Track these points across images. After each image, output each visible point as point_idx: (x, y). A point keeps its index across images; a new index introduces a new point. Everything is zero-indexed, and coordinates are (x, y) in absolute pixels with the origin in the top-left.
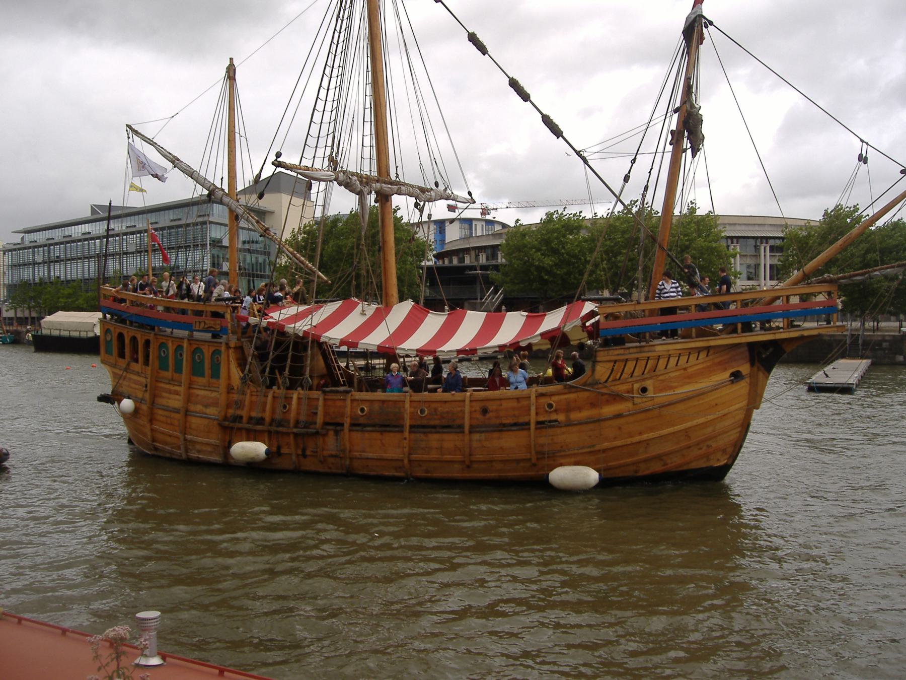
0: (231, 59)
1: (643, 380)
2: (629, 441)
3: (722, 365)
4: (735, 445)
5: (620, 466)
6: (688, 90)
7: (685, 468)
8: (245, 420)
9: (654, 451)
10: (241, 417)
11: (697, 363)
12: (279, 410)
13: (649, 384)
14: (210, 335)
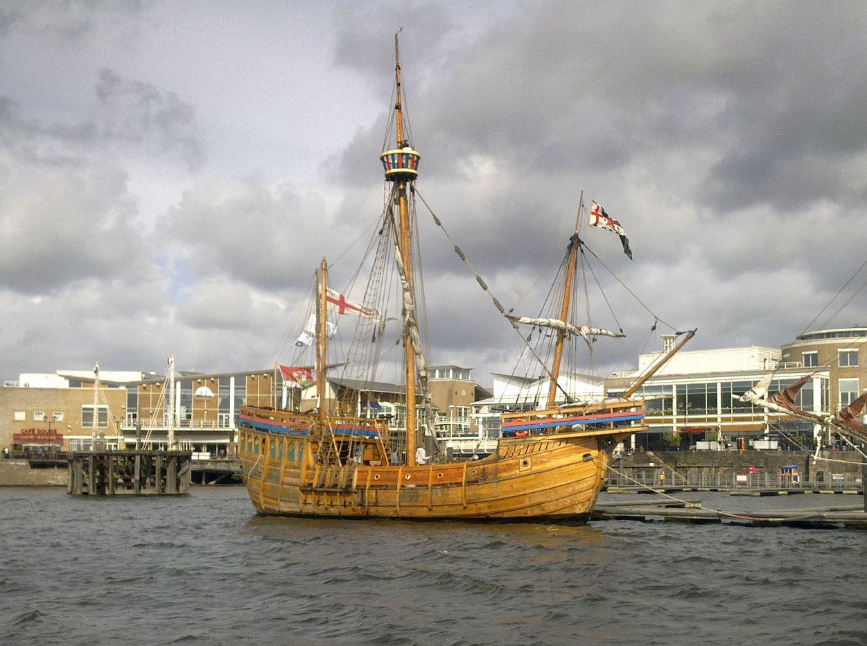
0: (697, 329)
1: (525, 457)
13: (528, 460)
14: (646, 519)
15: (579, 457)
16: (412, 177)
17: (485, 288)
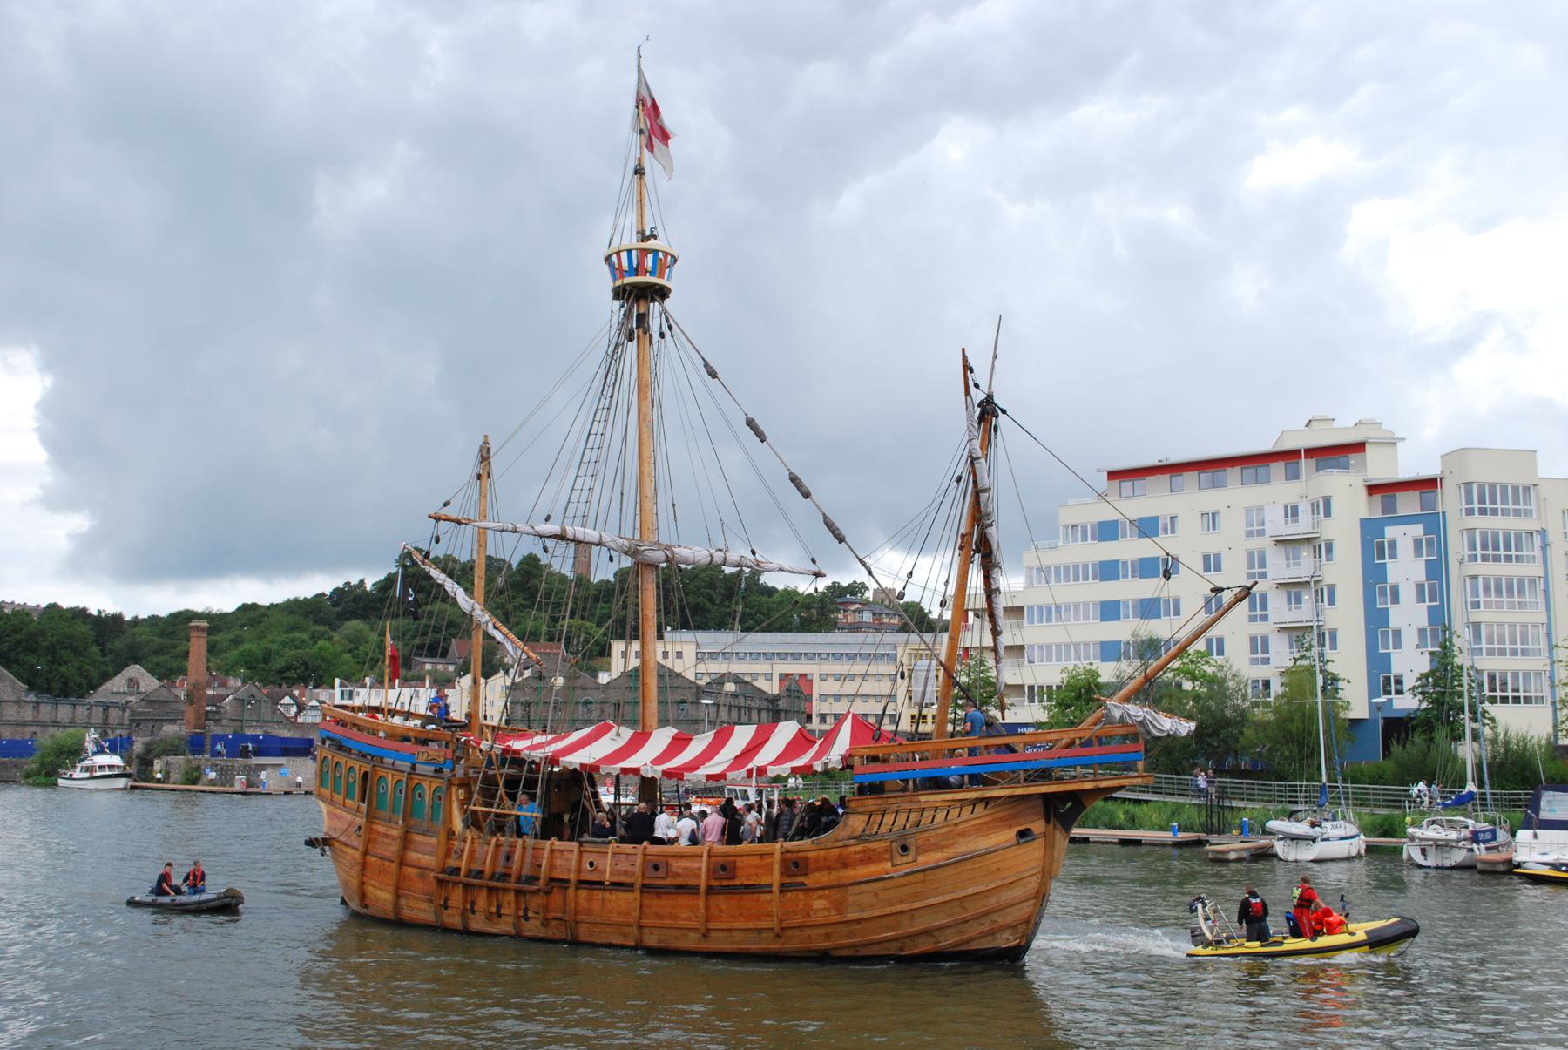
2: (888, 910)
3: (1007, 822)
5: (880, 942)
6: (639, 70)
7: (964, 948)
9: (922, 923)
12: (501, 861)
15: (1010, 834)
16: (662, 293)
17: (807, 495)
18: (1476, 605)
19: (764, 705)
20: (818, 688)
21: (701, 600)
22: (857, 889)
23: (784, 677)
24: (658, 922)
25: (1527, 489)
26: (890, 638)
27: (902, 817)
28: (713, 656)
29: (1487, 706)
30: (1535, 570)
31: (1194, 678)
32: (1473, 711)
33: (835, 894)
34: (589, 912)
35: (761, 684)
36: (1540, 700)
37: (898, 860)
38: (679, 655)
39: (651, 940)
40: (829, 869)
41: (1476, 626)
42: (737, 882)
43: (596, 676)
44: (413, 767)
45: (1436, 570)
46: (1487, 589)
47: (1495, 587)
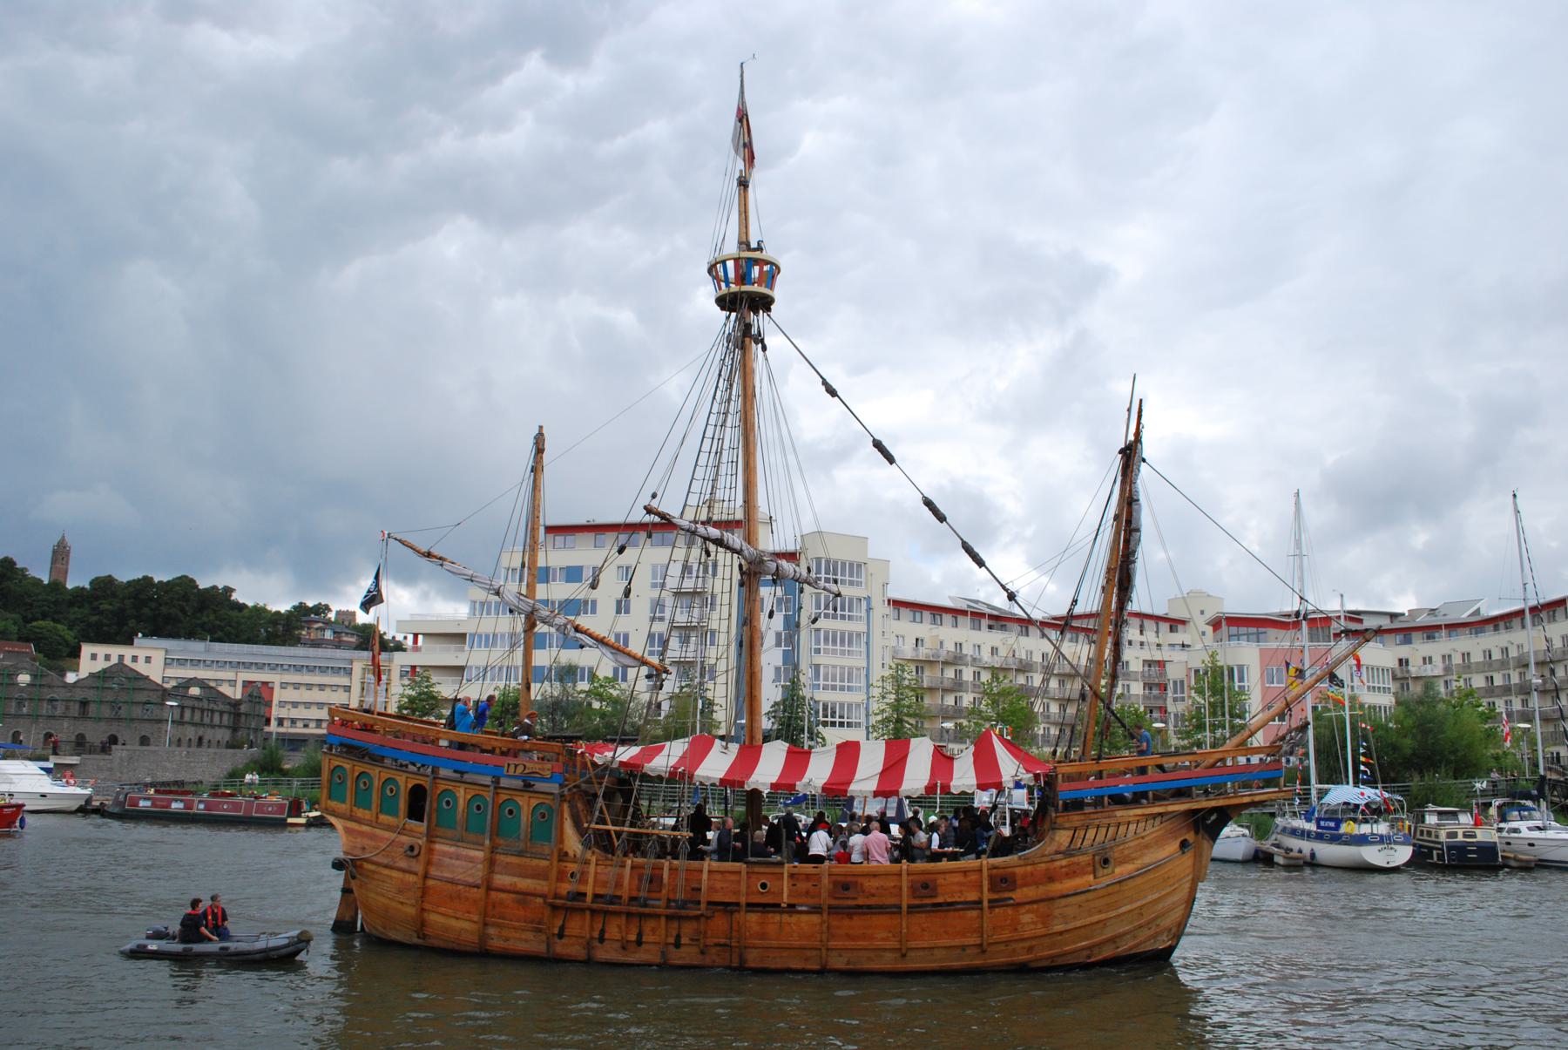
4: (1179, 925)
8: (589, 897)
10: (620, 897)
11: (1152, 830)
18: (818, 651)
19: (227, 708)
20: (279, 694)
21: (173, 611)
22: (1063, 902)
23: (247, 684)
24: (849, 944)
25: (859, 566)
26: (347, 654)
27: (1103, 831)
28: (182, 662)
29: (820, 728)
30: (860, 627)
31: (601, 700)
32: (810, 732)
33: (1042, 907)
34: (763, 936)
35: (225, 689)
36: (858, 725)
37: (1100, 872)
38: (148, 660)
39: (838, 962)
40: (1037, 884)
41: (817, 667)
42: (940, 900)
43: (64, 675)
44: (496, 781)
45: (792, 625)
46: (826, 640)
47: (832, 638)
